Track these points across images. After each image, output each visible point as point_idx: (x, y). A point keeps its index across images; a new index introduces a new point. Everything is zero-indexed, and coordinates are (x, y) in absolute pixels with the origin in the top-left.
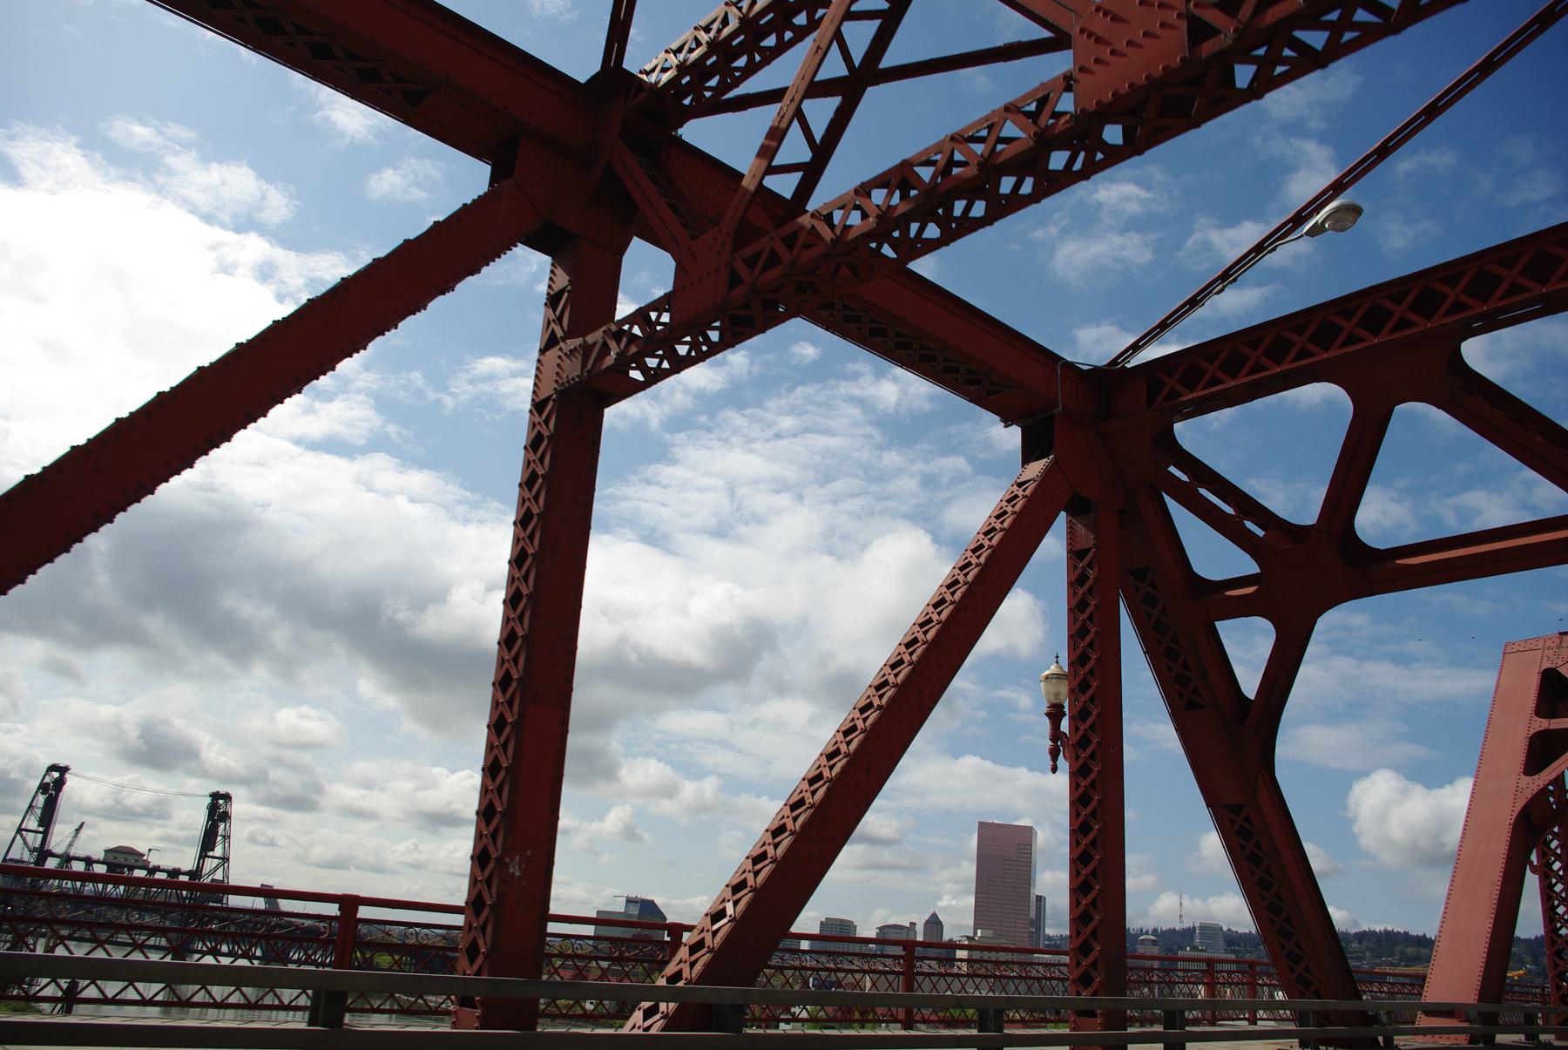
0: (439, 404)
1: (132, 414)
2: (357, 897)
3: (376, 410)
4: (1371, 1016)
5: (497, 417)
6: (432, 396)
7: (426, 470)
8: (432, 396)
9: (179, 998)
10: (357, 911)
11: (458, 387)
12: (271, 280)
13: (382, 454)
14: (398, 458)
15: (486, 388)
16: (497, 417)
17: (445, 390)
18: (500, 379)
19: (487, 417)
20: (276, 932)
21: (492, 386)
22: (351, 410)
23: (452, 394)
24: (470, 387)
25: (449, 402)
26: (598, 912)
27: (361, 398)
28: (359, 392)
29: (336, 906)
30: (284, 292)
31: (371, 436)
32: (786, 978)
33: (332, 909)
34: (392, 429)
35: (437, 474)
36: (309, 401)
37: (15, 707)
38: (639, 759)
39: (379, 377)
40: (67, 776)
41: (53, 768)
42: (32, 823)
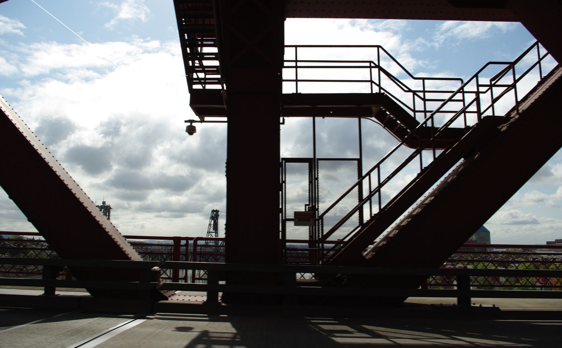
0: (433, 47)
1: (486, 116)
2: (180, 237)
3: (412, 57)
4: (533, 260)
5: (458, 44)
6: (429, 45)
7: (439, 74)
8: (429, 45)
9: (490, 284)
10: (180, 242)
11: (438, 38)
12: (356, 25)
13: (421, 73)
14: (428, 72)
15: (449, 34)
16: (458, 44)
17: (432, 41)
18: (452, 29)
19: (454, 45)
20: (454, 259)
21: (450, 32)
22: (403, 61)
23: (436, 41)
24: (443, 36)
25: (437, 45)
26: (555, 240)
27: (405, 55)
28: (403, 53)
29: (172, 241)
30: (362, 27)
31: (414, 68)
32: (475, 266)
33: (171, 242)
34: (420, 62)
35: (444, 73)
36: (388, 63)
37: (329, 192)
38: (558, 164)
39: (408, 44)
40: (219, 213)
41: (213, 211)
42: (212, 230)
